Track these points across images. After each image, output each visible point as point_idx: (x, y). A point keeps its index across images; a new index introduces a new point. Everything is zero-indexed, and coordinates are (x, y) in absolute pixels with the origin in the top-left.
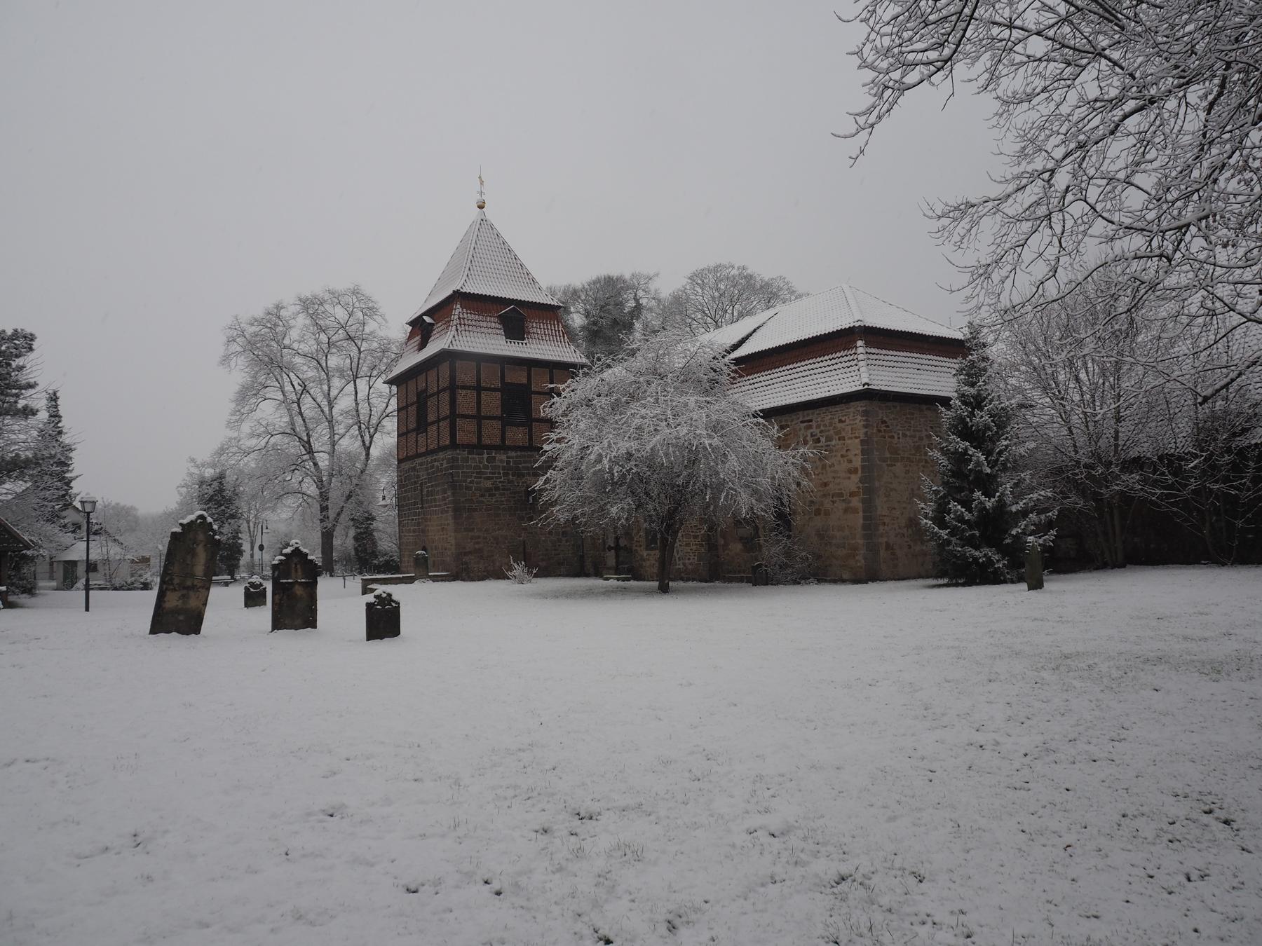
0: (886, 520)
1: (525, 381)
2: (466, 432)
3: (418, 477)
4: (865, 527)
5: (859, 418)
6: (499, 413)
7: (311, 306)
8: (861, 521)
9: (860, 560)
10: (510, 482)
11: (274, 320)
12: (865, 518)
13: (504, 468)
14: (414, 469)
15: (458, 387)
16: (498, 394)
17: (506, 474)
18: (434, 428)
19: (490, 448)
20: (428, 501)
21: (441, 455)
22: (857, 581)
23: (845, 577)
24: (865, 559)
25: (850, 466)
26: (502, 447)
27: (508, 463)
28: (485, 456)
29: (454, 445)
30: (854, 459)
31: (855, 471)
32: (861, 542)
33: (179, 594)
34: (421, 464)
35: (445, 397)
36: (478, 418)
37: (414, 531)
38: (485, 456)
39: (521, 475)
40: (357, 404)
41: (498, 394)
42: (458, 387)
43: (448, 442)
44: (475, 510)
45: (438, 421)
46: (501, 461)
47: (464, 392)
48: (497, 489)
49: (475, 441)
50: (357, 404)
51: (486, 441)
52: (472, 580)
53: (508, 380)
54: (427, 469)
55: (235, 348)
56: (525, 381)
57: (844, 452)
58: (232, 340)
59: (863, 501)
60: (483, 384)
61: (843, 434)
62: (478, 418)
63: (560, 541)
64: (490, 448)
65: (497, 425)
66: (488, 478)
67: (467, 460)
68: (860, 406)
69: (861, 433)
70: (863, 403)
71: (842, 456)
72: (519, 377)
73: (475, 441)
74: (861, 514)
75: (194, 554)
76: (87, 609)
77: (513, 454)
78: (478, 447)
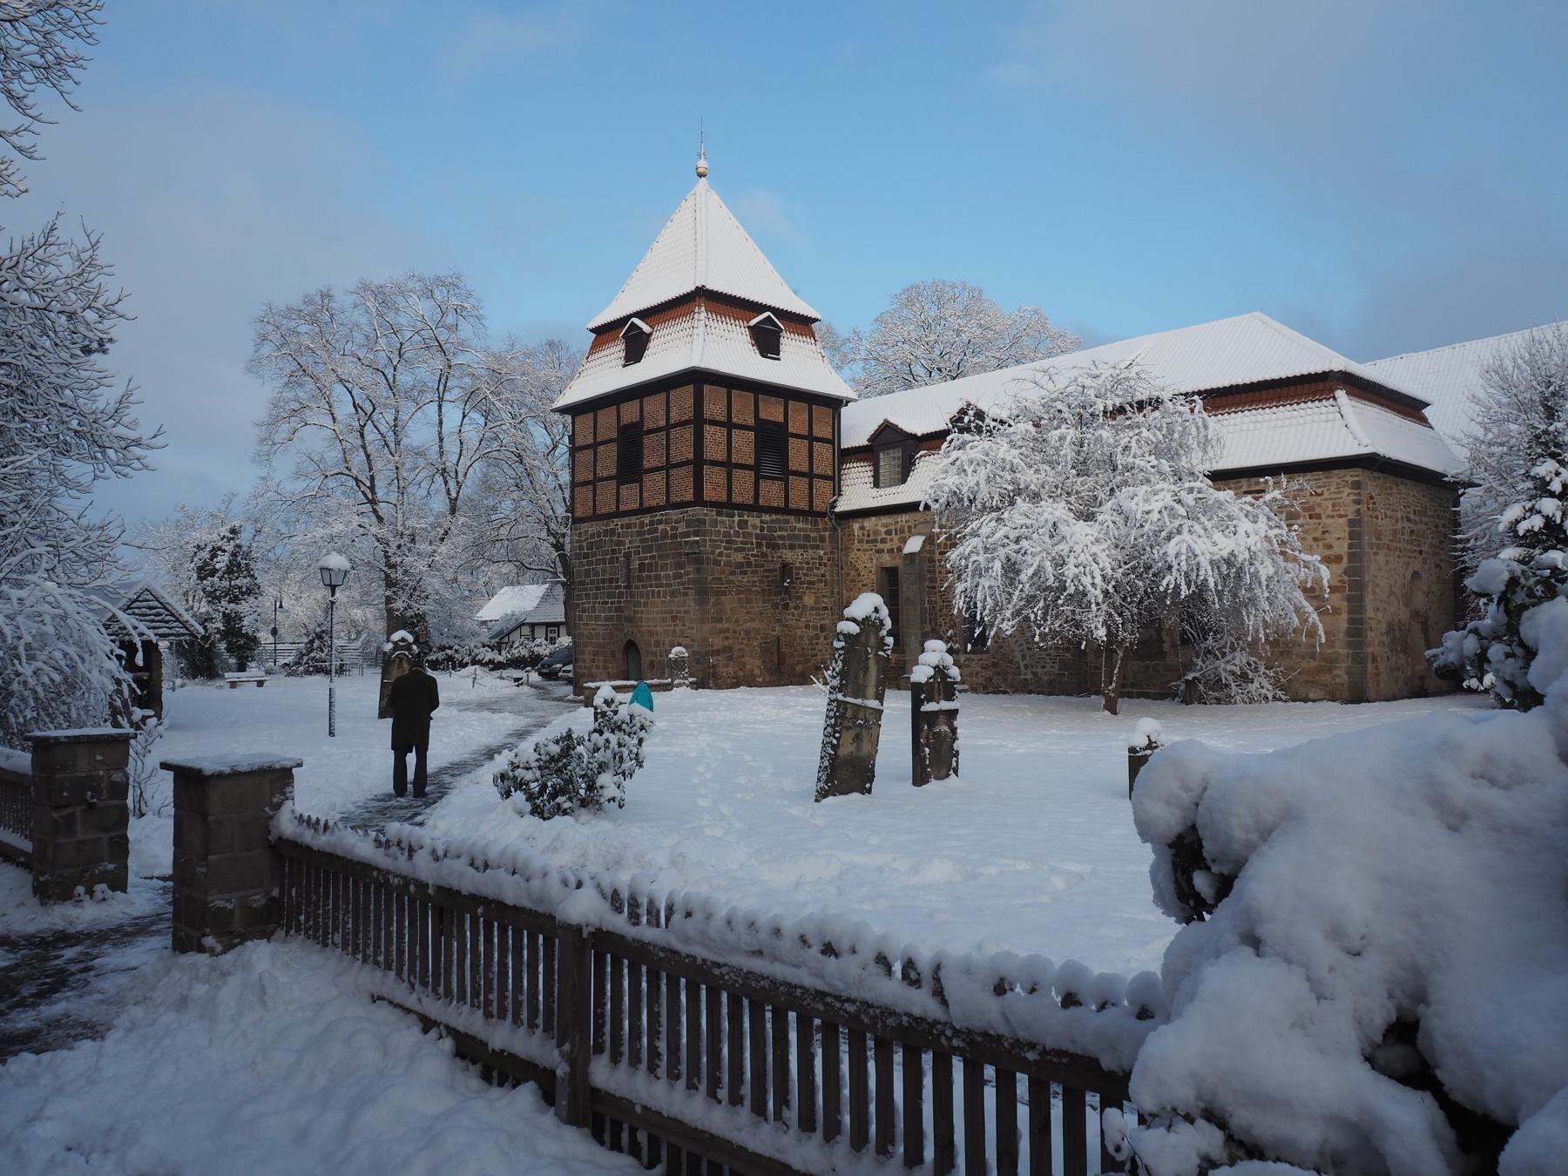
0: (1373, 623)
1: (781, 419)
2: (714, 480)
3: (620, 543)
4: (1349, 633)
5: (1347, 490)
6: (751, 462)
7: (384, 298)
8: (1345, 625)
9: (1341, 675)
10: (764, 555)
11: (319, 310)
12: (1350, 621)
13: (757, 536)
14: (612, 532)
15: (705, 422)
16: (751, 435)
17: (759, 545)
18: (659, 477)
19: (742, 507)
20: (640, 579)
21: (674, 514)
22: (1387, 700)
23: (1312, 696)
24: (1348, 673)
25: (1328, 552)
26: (755, 508)
27: (762, 529)
28: (736, 519)
29: (699, 500)
30: (1335, 544)
31: (1338, 559)
32: (1343, 651)
33: (853, 733)
34: (628, 526)
35: (688, 433)
36: (728, 465)
37: (607, 619)
38: (736, 519)
39: (775, 547)
40: (441, 440)
41: (751, 435)
42: (705, 422)
43: (689, 497)
44: (724, 593)
45: (668, 467)
46: (754, 527)
47: (713, 428)
48: (749, 564)
49: (724, 498)
50: (441, 440)
51: (737, 499)
52: (718, 687)
53: (763, 416)
54: (640, 533)
55: (267, 349)
56: (781, 419)
57: (1318, 534)
58: (264, 338)
59: (1349, 599)
60: (734, 420)
61: (1318, 510)
62: (728, 465)
63: (817, 637)
64: (742, 507)
65: (749, 476)
66: (738, 550)
67: (714, 523)
68: (1350, 475)
69: (1350, 511)
70: (1358, 471)
71: (1315, 539)
72: (772, 411)
73: (724, 498)
74: (1345, 616)
75: (867, 670)
76: (331, 734)
77: (767, 517)
78: (728, 506)
